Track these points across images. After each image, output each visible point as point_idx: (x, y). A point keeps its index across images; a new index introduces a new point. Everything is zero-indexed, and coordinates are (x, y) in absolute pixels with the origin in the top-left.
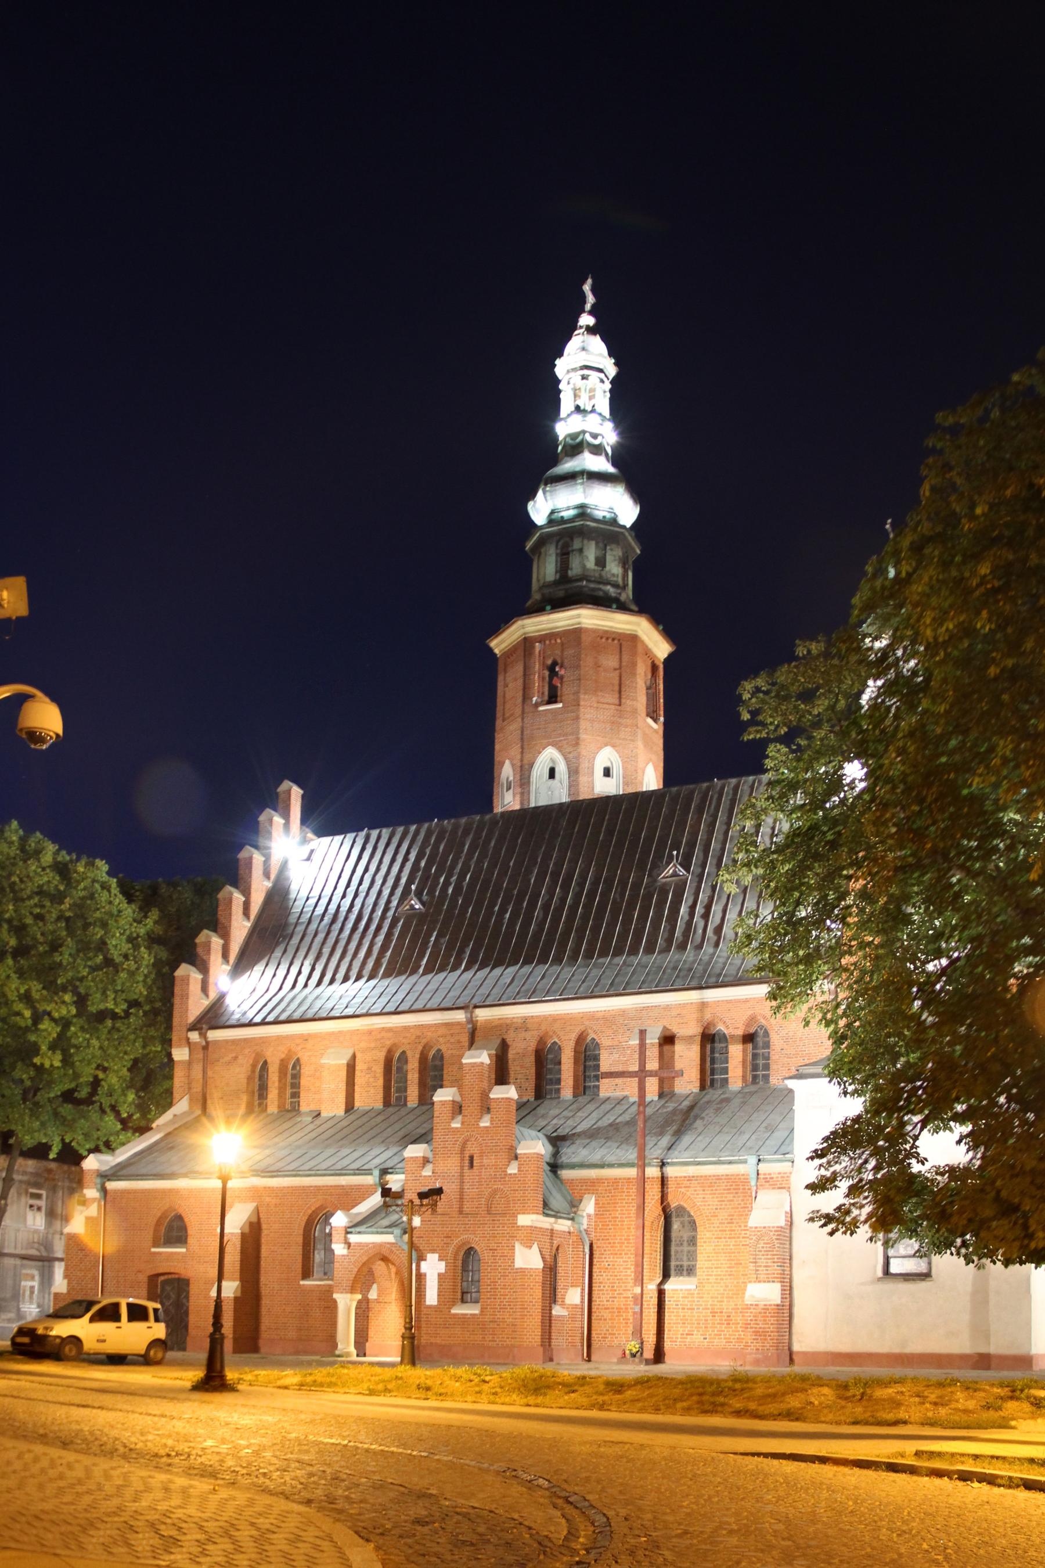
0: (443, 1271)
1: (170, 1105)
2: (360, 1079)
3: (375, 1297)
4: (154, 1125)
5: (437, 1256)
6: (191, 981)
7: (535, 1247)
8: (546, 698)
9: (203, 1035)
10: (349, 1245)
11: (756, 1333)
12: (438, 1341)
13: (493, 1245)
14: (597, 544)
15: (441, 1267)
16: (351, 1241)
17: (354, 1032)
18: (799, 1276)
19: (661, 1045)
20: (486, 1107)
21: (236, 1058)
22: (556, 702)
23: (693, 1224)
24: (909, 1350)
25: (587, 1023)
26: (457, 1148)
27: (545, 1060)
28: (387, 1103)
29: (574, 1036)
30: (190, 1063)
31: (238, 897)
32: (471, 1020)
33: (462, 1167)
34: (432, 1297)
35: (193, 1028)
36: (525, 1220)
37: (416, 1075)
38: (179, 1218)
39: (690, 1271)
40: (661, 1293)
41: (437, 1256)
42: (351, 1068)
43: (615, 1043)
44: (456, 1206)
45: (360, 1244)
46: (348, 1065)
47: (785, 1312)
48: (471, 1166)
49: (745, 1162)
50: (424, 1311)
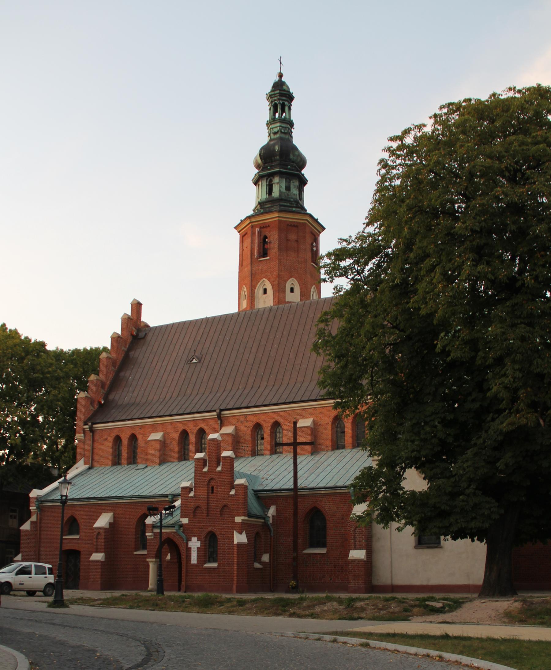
0: (199, 546)
5: (196, 538)
7: (244, 533)
8: (262, 254)
14: (286, 179)
15: (199, 544)
21: (107, 439)
22: (267, 257)
33: (208, 493)
37: (194, 446)
41: (196, 538)
48: (213, 492)
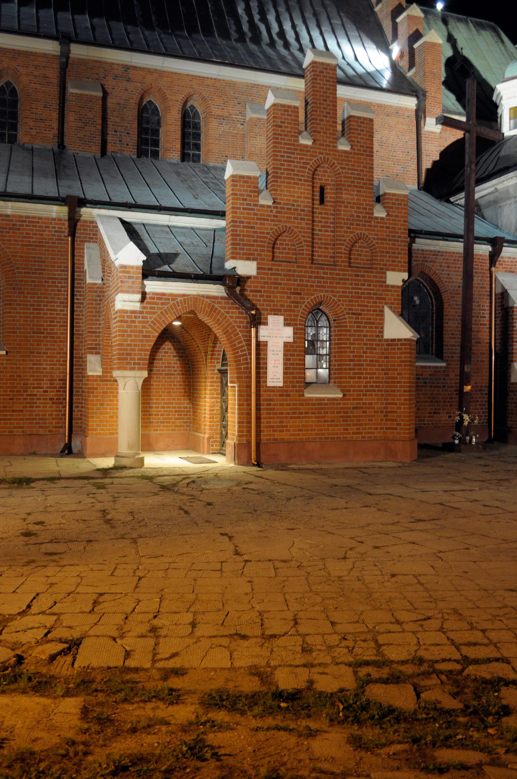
0: (291, 340)
3: (99, 372)
12: (286, 436)
13: (356, 308)
16: (147, 290)
25: (196, 87)
26: (307, 173)
43: (226, 114)
44: (307, 251)
45: (161, 296)
48: (322, 201)
50: (264, 395)
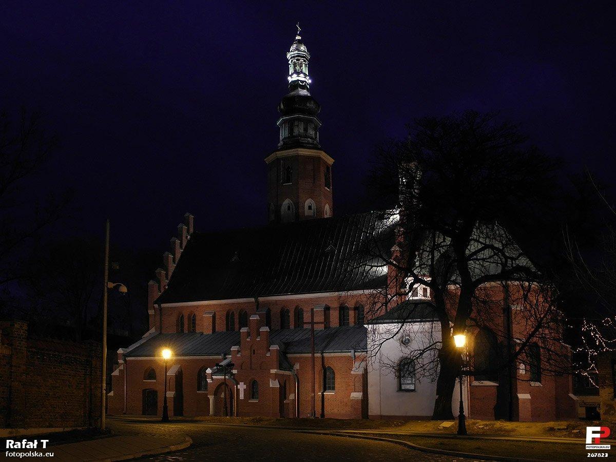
1: (148, 330)
2: (217, 321)
4: (142, 337)
6: (169, 258)
9: (159, 306)
10: (212, 379)
11: (355, 409)
17: (214, 305)
18: (370, 390)
19: (325, 311)
20: (259, 334)
23: (334, 373)
24: (408, 415)
27: (284, 313)
28: (227, 329)
29: (294, 307)
30: (155, 315)
31: (178, 242)
32: (257, 301)
34: (242, 396)
35: (156, 303)
36: (273, 371)
37: (238, 320)
38: (153, 370)
39: (333, 388)
40: (323, 395)
42: (214, 317)
46: (213, 316)
47: (365, 400)
48: (254, 354)
49: (350, 352)
